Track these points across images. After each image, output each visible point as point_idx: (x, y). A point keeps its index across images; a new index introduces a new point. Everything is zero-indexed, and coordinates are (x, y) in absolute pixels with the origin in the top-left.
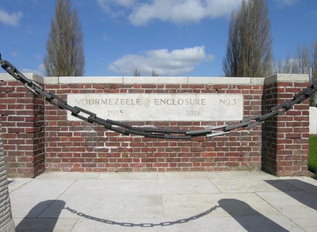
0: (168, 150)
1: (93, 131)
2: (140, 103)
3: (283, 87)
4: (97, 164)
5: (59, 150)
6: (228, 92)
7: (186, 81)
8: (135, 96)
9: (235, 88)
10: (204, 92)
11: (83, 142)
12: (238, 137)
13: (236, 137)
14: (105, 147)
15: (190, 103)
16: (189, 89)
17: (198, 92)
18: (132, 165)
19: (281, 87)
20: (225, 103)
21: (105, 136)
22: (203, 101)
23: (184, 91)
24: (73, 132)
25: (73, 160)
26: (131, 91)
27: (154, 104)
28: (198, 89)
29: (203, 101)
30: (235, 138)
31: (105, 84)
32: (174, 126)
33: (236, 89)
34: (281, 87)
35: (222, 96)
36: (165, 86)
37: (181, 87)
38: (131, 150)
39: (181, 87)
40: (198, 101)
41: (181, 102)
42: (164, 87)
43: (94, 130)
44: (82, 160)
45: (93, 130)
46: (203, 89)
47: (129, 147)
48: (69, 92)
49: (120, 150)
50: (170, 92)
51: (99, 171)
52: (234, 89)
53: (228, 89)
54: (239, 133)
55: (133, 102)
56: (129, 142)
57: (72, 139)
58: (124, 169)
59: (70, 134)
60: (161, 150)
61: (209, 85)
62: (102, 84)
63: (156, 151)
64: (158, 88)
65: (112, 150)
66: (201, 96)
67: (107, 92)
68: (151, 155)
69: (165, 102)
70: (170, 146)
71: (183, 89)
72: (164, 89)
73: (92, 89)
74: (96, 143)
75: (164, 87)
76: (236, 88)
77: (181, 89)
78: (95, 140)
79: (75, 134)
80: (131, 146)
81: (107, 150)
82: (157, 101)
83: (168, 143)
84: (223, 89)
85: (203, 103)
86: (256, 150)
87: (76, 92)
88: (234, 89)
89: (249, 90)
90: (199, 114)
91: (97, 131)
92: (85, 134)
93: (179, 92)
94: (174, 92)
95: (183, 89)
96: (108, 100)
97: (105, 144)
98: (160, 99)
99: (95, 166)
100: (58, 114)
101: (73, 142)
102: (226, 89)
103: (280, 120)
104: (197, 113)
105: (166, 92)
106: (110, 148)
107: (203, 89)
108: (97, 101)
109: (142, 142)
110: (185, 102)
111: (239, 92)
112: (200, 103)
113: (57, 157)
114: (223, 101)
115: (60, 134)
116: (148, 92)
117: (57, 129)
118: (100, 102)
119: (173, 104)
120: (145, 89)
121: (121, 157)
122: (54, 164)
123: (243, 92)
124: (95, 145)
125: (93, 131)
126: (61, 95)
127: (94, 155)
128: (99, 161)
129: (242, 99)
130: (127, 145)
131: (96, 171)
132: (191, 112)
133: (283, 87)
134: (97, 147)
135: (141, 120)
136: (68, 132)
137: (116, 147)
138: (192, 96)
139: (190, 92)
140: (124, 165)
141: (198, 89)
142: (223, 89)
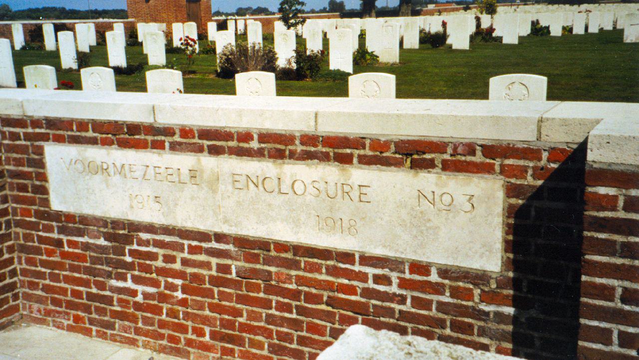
0: (270, 319)
1: (102, 242)
2: (198, 180)
3: (611, 191)
4: (118, 323)
5: (41, 275)
6: (446, 166)
7: (312, 123)
8: (184, 161)
9: (473, 152)
10: (366, 161)
11: (85, 264)
12: (482, 324)
13: (477, 324)
14: (130, 284)
15: (323, 195)
16: (320, 148)
17: (345, 160)
18: (189, 343)
19: (602, 190)
20: (439, 205)
21: (129, 259)
22: (364, 190)
23: (307, 156)
24: (64, 238)
25: (71, 305)
26: (174, 147)
27: (230, 188)
28: (348, 151)
29: (364, 190)
30: (471, 326)
31: (116, 122)
32: (283, 255)
33: (479, 158)
34: (602, 190)
35: (428, 180)
36: (256, 137)
37: (297, 142)
38: (183, 303)
39: (297, 142)
40: (347, 189)
41: (299, 188)
42: (252, 139)
43: (106, 239)
44: (87, 309)
45: (102, 239)
46: (362, 152)
47: (179, 295)
48: (45, 138)
49: (163, 298)
50: (270, 157)
51: (121, 342)
52: (469, 158)
53: (446, 157)
54: (487, 314)
55: (182, 178)
56: (178, 282)
57: (64, 255)
58: (171, 347)
59: (59, 243)
60: (253, 316)
61: (383, 139)
62: (110, 123)
63: (241, 316)
64: (239, 140)
65: (146, 296)
66: (359, 174)
67: (124, 144)
68: (230, 325)
69: (261, 182)
70: (277, 309)
71: (304, 148)
72: (255, 145)
73: (90, 134)
74: (111, 273)
75: (252, 139)
76: (479, 153)
77: (299, 148)
78: (108, 264)
79: (71, 244)
80: (183, 292)
81: (134, 293)
82: (237, 178)
83: (271, 301)
84: (428, 156)
85: (363, 198)
86: (255, 319)
87: (59, 139)
88: (469, 158)
89: (531, 164)
90: (351, 230)
91: (111, 242)
92: (86, 247)
93: (292, 155)
94: (279, 155)
95: (304, 148)
96: (127, 168)
97: (129, 276)
98: (245, 173)
99: (111, 326)
100: (33, 192)
101: (68, 262)
102: (438, 158)
103: (500, 317)
104: (346, 224)
105: (259, 154)
106: (140, 288)
107: (362, 152)
108: (105, 166)
109: (207, 286)
110: (310, 189)
111: (487, 169)
112: (355, 194)
113: (40, 293)
114: (430, 197)
115: (41, 240)
116: (215, 151)
117: (34, 226)
118: (111, 170)
119: (280, 192)
120: (206, 143)
121: (164, 317)
122: (36, 306)
123: (504, 171)
124: (109, 275)
125: (102, 242)
126: (32, 145)
127: (109, 301)
128: (122, 316)
129: (500, 194)
130: (173, 288)
131: (115, 341)
132: (330, 222)
133: (611, 191)
134: (114, 283)
135: (202, 227)
136: (55, 235)
137: (151, 290)
138: (329, 172)
139: (324, 158)
140: (172, 339)
141: (348, 151)
142: (428, 156)
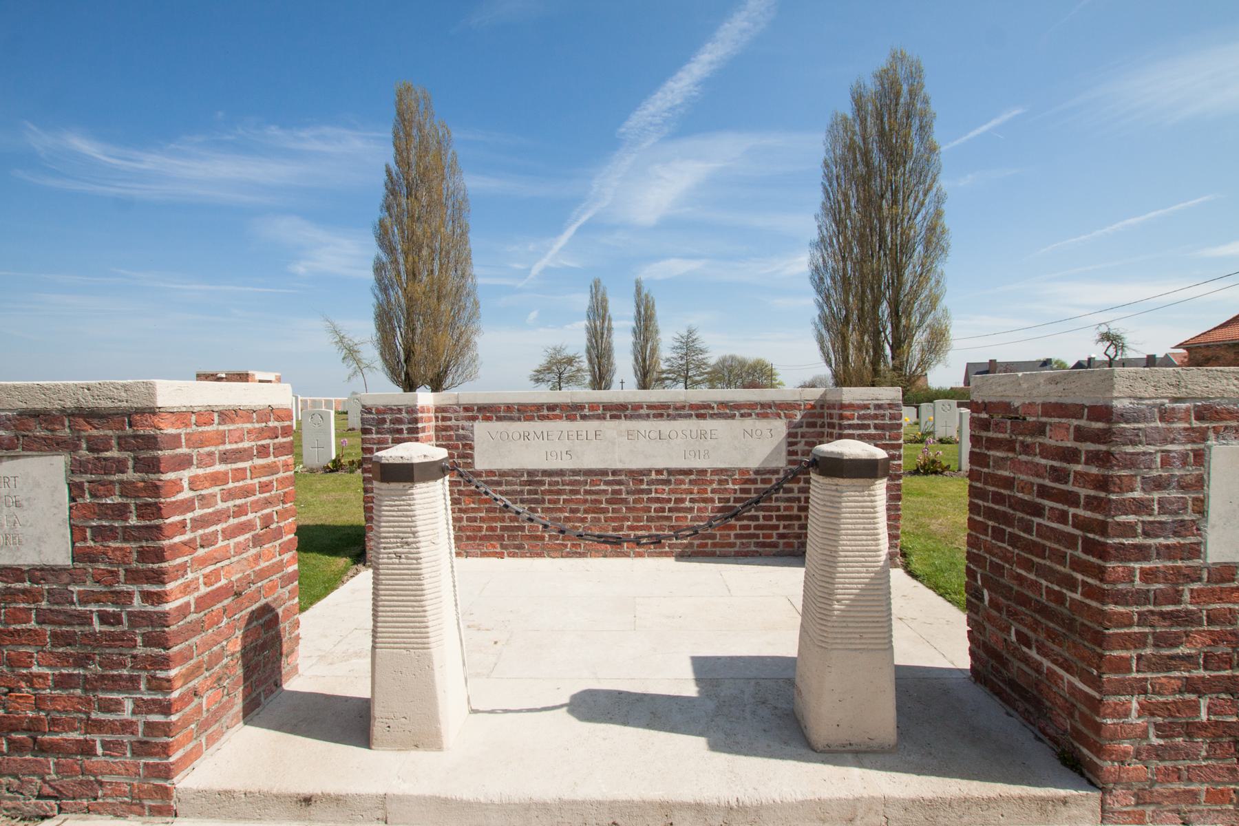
138: (693, 425)
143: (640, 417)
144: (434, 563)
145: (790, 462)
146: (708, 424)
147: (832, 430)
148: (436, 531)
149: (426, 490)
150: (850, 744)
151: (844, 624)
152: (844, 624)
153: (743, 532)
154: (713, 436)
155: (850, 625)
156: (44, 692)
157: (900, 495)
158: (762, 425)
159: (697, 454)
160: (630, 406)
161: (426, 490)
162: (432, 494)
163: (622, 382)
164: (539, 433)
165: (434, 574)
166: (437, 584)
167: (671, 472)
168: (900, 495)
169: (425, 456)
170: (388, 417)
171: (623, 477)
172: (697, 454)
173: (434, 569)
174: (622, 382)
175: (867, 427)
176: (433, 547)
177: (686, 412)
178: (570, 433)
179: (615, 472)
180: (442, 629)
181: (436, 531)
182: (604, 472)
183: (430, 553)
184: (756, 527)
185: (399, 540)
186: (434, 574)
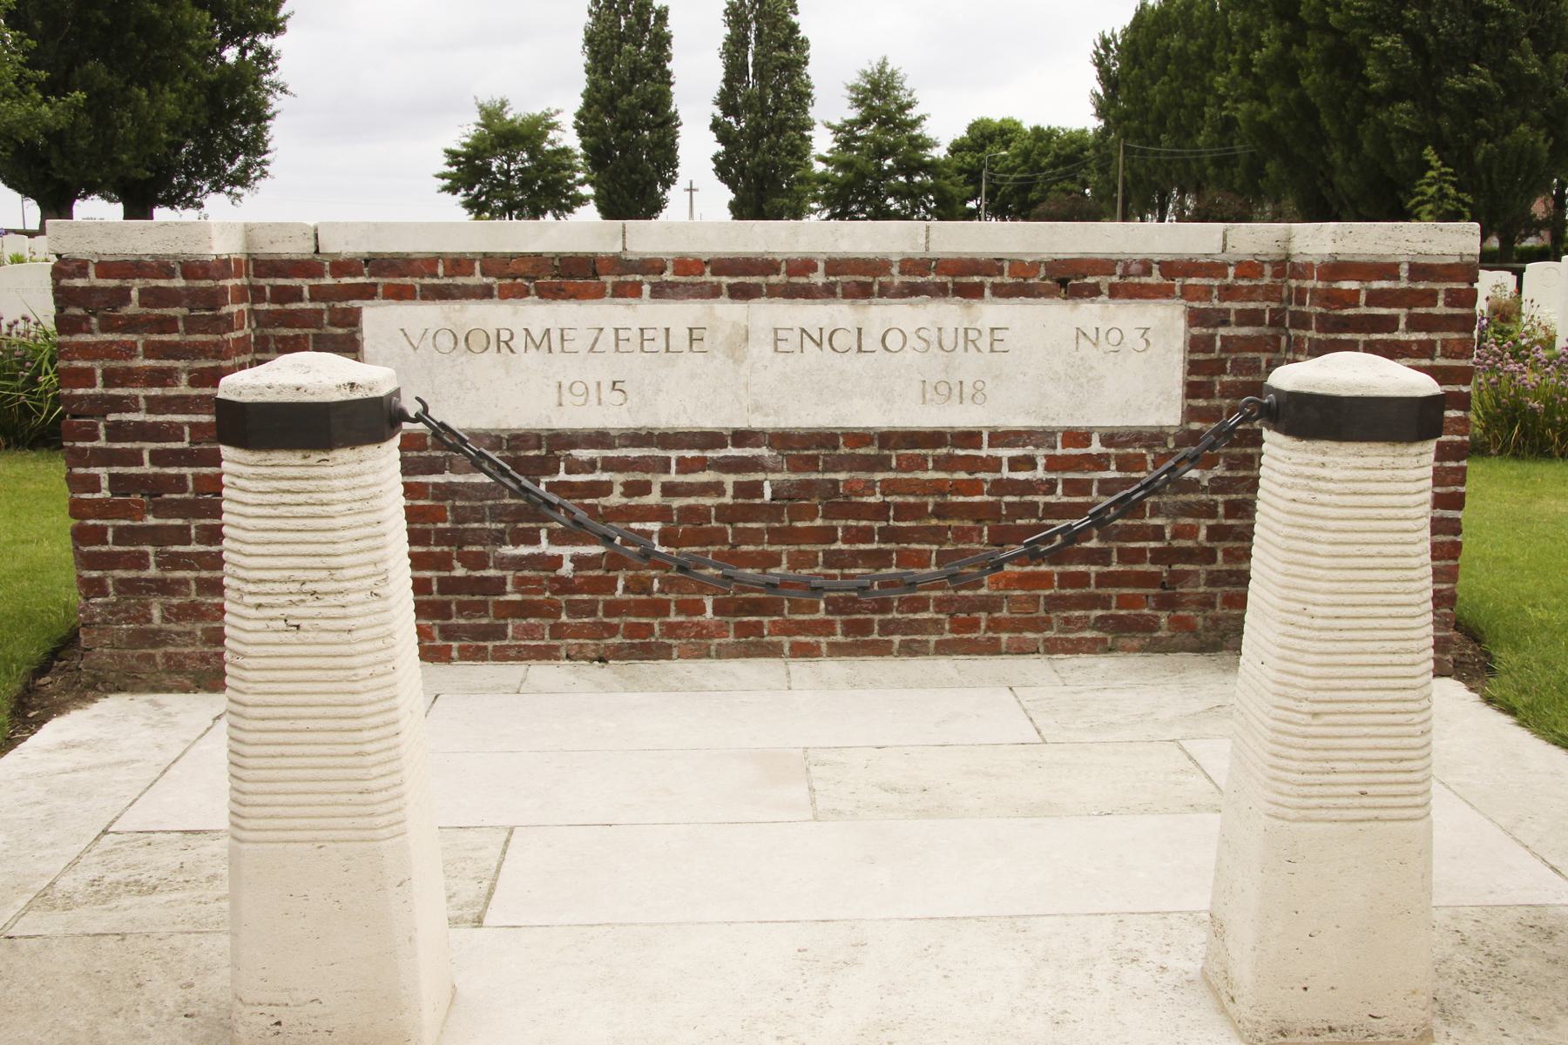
138: (947, 314)
143: (808, 293)
144: (379, 644)
145: (1191, 414)
146: (991, 312)
147: (1302, 333)
148: (381, 567)
149: (356, 468)
150: (1331, 1029)
151: (1328, 766)
152: (1328, 766)
153: (1068, 592)
154: (997, 346)
155: (1339, 766)
156: (541, 597)
157: (1463, 495)
158: (1130, 317)
159: (954, 391)
160: (1006, 265)
161: (356, 468)
162: (370, 479)
163: (691, 190)
164: (537, 334)
165: (380, 669)
166: (387, 693)
167: (889, 439)
168: (1463, 495)
169: (352, 385)
170: (136, 285)
171: (764, 451)
172: (956, 391)
173: (382, 655)
174: (691, 190)
175: (1390, 324)
176: (377, 605)
177: (477, 279)
178: (622, 334)
179: (742, 437)
180: (399, 796)
181: (381, 567)
182: (713, 439)
183: (372, 619)
184: (1103, 579)
185: (294, 587)
186: (380, 669)
